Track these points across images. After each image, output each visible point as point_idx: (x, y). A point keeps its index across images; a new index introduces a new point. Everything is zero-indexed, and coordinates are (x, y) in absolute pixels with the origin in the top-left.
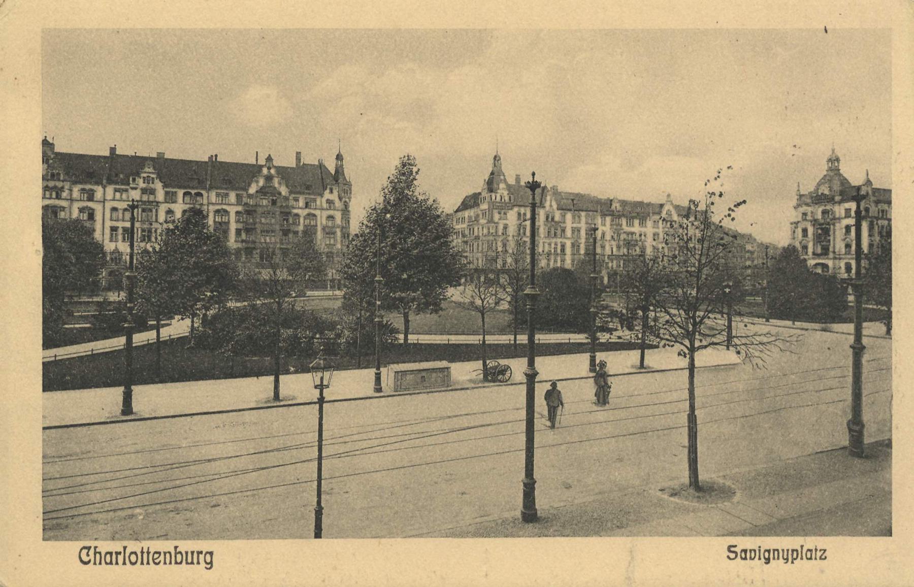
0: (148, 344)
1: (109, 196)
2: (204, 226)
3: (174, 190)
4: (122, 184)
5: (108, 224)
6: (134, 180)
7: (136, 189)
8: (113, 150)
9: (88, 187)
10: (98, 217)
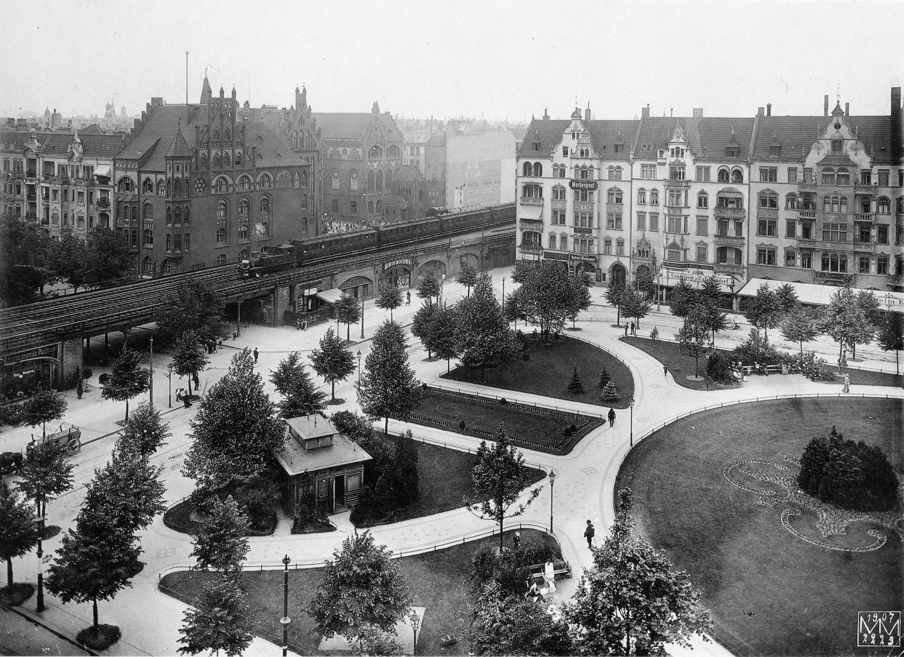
0: (464, 543)
1: (637, 173)
2: (263, 525)
3: (707, 165)
4: (649, 159)
5: (636, 208)
6: (662, 152)
7: (664, 164)
8: (646, 111)
9: (615, 164)
10: (626, 199)
